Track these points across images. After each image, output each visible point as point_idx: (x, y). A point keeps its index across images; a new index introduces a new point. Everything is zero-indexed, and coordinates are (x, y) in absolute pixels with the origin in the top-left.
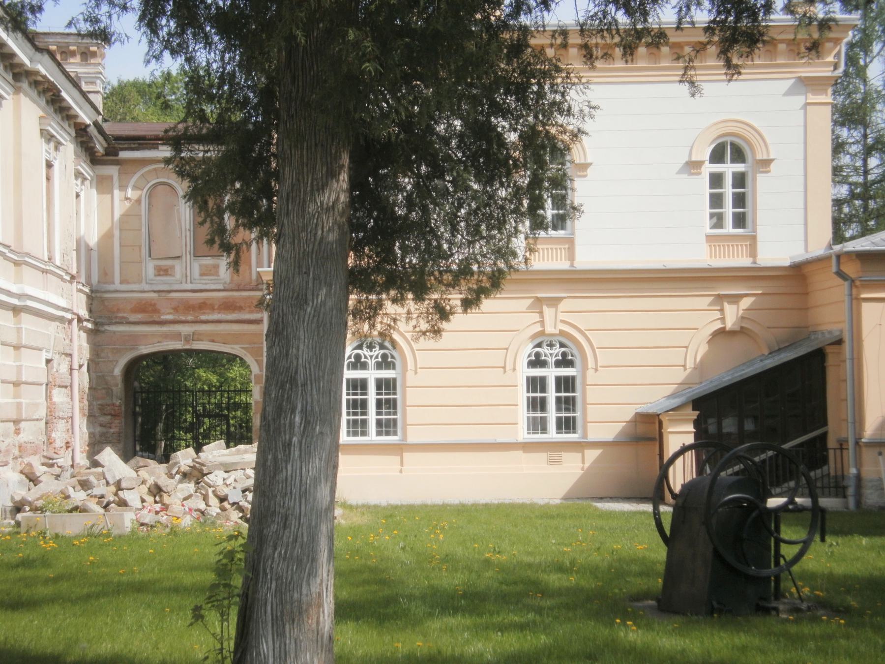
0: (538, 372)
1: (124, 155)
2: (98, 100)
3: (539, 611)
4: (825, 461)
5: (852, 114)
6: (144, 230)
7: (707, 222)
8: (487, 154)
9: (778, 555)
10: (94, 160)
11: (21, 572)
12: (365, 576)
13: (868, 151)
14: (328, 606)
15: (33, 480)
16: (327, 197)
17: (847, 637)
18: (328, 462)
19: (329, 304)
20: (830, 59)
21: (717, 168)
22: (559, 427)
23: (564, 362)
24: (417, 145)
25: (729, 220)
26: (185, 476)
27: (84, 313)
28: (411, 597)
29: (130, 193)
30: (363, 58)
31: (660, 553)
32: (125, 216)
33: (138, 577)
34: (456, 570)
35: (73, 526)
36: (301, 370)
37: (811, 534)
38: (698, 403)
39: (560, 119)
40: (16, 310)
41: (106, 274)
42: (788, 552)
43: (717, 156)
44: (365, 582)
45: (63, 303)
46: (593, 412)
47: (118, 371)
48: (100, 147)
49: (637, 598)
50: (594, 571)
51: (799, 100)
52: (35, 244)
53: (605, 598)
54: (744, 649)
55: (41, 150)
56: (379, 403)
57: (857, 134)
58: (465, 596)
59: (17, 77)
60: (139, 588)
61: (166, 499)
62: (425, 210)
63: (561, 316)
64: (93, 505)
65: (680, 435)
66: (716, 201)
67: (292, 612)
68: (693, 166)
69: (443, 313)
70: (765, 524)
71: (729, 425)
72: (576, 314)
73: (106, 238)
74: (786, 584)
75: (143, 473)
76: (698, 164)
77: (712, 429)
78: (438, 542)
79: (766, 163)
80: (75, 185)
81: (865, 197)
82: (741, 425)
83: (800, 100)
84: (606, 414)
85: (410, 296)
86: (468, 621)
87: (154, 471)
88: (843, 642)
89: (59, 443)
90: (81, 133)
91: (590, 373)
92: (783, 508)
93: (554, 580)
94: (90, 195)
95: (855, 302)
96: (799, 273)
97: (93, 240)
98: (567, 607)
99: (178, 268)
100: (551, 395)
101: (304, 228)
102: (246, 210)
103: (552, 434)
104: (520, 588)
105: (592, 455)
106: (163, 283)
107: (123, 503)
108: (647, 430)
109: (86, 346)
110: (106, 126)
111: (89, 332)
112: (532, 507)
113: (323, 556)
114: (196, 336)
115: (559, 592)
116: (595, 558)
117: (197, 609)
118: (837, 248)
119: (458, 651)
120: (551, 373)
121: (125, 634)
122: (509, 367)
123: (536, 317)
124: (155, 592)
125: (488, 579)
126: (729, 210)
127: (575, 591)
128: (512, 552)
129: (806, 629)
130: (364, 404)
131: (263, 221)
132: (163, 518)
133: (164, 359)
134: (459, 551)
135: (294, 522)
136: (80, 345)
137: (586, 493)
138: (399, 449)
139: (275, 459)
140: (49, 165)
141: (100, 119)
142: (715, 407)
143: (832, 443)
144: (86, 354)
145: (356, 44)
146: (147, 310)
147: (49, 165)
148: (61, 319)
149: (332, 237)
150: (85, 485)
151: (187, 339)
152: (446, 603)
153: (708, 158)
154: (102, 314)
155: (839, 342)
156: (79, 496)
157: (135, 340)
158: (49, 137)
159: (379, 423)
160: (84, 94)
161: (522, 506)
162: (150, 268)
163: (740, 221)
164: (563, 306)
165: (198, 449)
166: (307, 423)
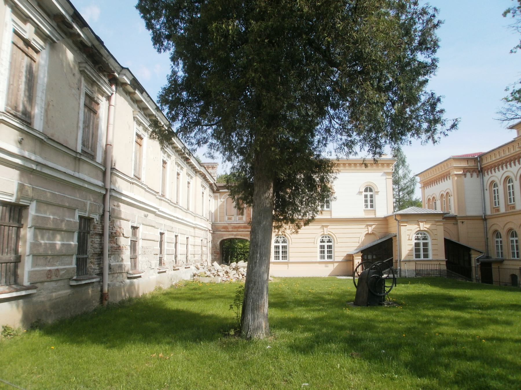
0: (323, 244)
1: (221, 191)
2: (215, 178)
3: (323, 306)
4: (392, 265)
5: (396, 182)
6: (225, 209)
7: (364, 207)
8: (311, 184)
9: (384, 290)
10: (214, 192)
11: (194, 291)
12: (278, 296)
13: (399, 191)
14: (267, 305)
15: (198, 269)
16: (267, 195)
17: (403, 312)
18: (267, 267)
19: (267, 224)
20: (391, 168)
21: (366, 193)
22: (328, 258)
23: (329, 241)
24: (291, 181)
25: (369, 206)
26: (234, 269)
27: (210, 229)
28: (289, 302)
29: (222, 200)
30: (276, 155)
31: (354, 290)
32: (221, 206)
33: (221, 294)
34: (301, 294)
35: (206, 280)
36: (259, 242)
37: (393, 285)
38: (362, 251)
39: (330, 175)
40: (194, 228)
41: (216, 219)
42: (387, 289)
43: (366, 190)
44: (278, 297)
45: (205, 226)
46: (336, 254)
47: (218, 243)
48: (215, 189)
49: (348, 302)
50: (337, 295)
51: (384, 177)
52: (199, 212)
53: (340, 302)
54: (377, 315)
55: (201, 189)
56: (282, 252)
57: (397, 187)
58: (304, 301)
59: (196, 172)
60: (221, 297)
61: (229, 275)
62: (294, 199)
63: (328, 230)
64: (211, 275)
65: (358, 260)
66: (366, 201)
67: (257, 308)
68: (360, 193)
69: (299, 228)
70: (381, 282)
71: (370, 257)
72: (332, 230)
73: (216, 210)
74: (386, 297)
75: (223, 268)
76: (362, 192)
77: (365, 258)
78: (297, 287)
79: (378, 192)
80: (209, 198)
81: (399, 202)
82: (373, 257)
83: (385, 177)
84: (339, 255)
85: (290, 222)
86: (305, 308)
87: (226, 268)
88: (402, 313)
89: (204, 260)
90: (211, 185)
91: (336, 244)
92: (386, 278)
93: (327, 297)
94: (213, 200)
95: (399, 226)
96: (386, 220)
97: (213, 211)
98: (330, 304)
99: (233, 218)
100: (326, 250)
101: (261, 203)
102: (245, 199)
103: (326, 259)
104: (318, 299)
105: (336, 265)
106: (230, 222)
107: (219, 275)
108: (350, 258)
109: (211, 237)
110: (217, 184)
111: (212, 234)
112: (321, 278)
113: (265, 293)
114: (237, 235)
115: (328, 300)
116: (337, 291)
117: (231, 305)
118: (395, 213)
119: (302, 317)
120: (326, 244)
121: (216, 309)
122: (315, 242)
123: (322, 230)
124: (225, 298)
125: (310, 297)
126: (369, 204)
127: (333, 300)
128: (316, 290)
129: (392, 309)
130: (279, 252)
131: (250, 202)
132: (228, 279)
133: (231, 240)
134: (303, 289)
135: (257, 283)
136: (210, 237)
137: (334, 274)
138: (288, 263)
139: (252, 266)
140: (203, 193)
141: (215, 182)
142: (365, 252)
143: (394, 261)
144: (211, 239)
145: (274, 151)
146: (225, 228)
147: (203, 193)
148: (205, 230)
149: (268, 206)
150: (210, 270)
151: (235, 235)
152: (299, 303)
153: (363, 191)
154: (215, 229)
155: (396, 236)
156: (208, 273)
157: (222, 235)
158: (203, 186)
159: (282, 257)
160: (212, 177)
161: (318, 278)
162: (226, 218)
163: (372, 206)
164: (329, 227)
165: (237, 263)
166: (261, 257)
